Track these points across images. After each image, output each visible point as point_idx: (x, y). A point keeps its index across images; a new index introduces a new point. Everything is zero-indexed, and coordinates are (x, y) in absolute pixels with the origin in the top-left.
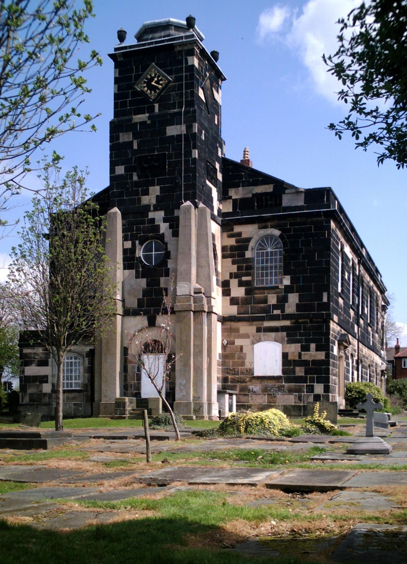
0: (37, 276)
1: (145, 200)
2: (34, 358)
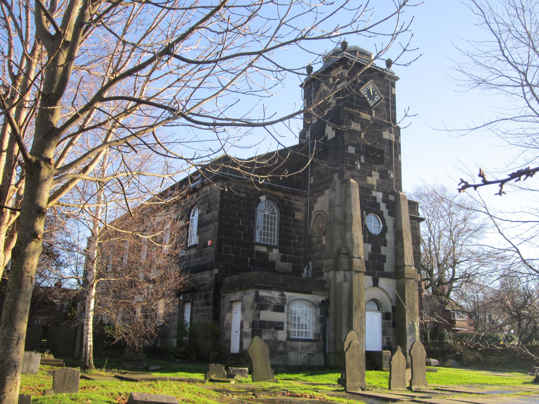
0: (46, 278)
2: (270, 302)
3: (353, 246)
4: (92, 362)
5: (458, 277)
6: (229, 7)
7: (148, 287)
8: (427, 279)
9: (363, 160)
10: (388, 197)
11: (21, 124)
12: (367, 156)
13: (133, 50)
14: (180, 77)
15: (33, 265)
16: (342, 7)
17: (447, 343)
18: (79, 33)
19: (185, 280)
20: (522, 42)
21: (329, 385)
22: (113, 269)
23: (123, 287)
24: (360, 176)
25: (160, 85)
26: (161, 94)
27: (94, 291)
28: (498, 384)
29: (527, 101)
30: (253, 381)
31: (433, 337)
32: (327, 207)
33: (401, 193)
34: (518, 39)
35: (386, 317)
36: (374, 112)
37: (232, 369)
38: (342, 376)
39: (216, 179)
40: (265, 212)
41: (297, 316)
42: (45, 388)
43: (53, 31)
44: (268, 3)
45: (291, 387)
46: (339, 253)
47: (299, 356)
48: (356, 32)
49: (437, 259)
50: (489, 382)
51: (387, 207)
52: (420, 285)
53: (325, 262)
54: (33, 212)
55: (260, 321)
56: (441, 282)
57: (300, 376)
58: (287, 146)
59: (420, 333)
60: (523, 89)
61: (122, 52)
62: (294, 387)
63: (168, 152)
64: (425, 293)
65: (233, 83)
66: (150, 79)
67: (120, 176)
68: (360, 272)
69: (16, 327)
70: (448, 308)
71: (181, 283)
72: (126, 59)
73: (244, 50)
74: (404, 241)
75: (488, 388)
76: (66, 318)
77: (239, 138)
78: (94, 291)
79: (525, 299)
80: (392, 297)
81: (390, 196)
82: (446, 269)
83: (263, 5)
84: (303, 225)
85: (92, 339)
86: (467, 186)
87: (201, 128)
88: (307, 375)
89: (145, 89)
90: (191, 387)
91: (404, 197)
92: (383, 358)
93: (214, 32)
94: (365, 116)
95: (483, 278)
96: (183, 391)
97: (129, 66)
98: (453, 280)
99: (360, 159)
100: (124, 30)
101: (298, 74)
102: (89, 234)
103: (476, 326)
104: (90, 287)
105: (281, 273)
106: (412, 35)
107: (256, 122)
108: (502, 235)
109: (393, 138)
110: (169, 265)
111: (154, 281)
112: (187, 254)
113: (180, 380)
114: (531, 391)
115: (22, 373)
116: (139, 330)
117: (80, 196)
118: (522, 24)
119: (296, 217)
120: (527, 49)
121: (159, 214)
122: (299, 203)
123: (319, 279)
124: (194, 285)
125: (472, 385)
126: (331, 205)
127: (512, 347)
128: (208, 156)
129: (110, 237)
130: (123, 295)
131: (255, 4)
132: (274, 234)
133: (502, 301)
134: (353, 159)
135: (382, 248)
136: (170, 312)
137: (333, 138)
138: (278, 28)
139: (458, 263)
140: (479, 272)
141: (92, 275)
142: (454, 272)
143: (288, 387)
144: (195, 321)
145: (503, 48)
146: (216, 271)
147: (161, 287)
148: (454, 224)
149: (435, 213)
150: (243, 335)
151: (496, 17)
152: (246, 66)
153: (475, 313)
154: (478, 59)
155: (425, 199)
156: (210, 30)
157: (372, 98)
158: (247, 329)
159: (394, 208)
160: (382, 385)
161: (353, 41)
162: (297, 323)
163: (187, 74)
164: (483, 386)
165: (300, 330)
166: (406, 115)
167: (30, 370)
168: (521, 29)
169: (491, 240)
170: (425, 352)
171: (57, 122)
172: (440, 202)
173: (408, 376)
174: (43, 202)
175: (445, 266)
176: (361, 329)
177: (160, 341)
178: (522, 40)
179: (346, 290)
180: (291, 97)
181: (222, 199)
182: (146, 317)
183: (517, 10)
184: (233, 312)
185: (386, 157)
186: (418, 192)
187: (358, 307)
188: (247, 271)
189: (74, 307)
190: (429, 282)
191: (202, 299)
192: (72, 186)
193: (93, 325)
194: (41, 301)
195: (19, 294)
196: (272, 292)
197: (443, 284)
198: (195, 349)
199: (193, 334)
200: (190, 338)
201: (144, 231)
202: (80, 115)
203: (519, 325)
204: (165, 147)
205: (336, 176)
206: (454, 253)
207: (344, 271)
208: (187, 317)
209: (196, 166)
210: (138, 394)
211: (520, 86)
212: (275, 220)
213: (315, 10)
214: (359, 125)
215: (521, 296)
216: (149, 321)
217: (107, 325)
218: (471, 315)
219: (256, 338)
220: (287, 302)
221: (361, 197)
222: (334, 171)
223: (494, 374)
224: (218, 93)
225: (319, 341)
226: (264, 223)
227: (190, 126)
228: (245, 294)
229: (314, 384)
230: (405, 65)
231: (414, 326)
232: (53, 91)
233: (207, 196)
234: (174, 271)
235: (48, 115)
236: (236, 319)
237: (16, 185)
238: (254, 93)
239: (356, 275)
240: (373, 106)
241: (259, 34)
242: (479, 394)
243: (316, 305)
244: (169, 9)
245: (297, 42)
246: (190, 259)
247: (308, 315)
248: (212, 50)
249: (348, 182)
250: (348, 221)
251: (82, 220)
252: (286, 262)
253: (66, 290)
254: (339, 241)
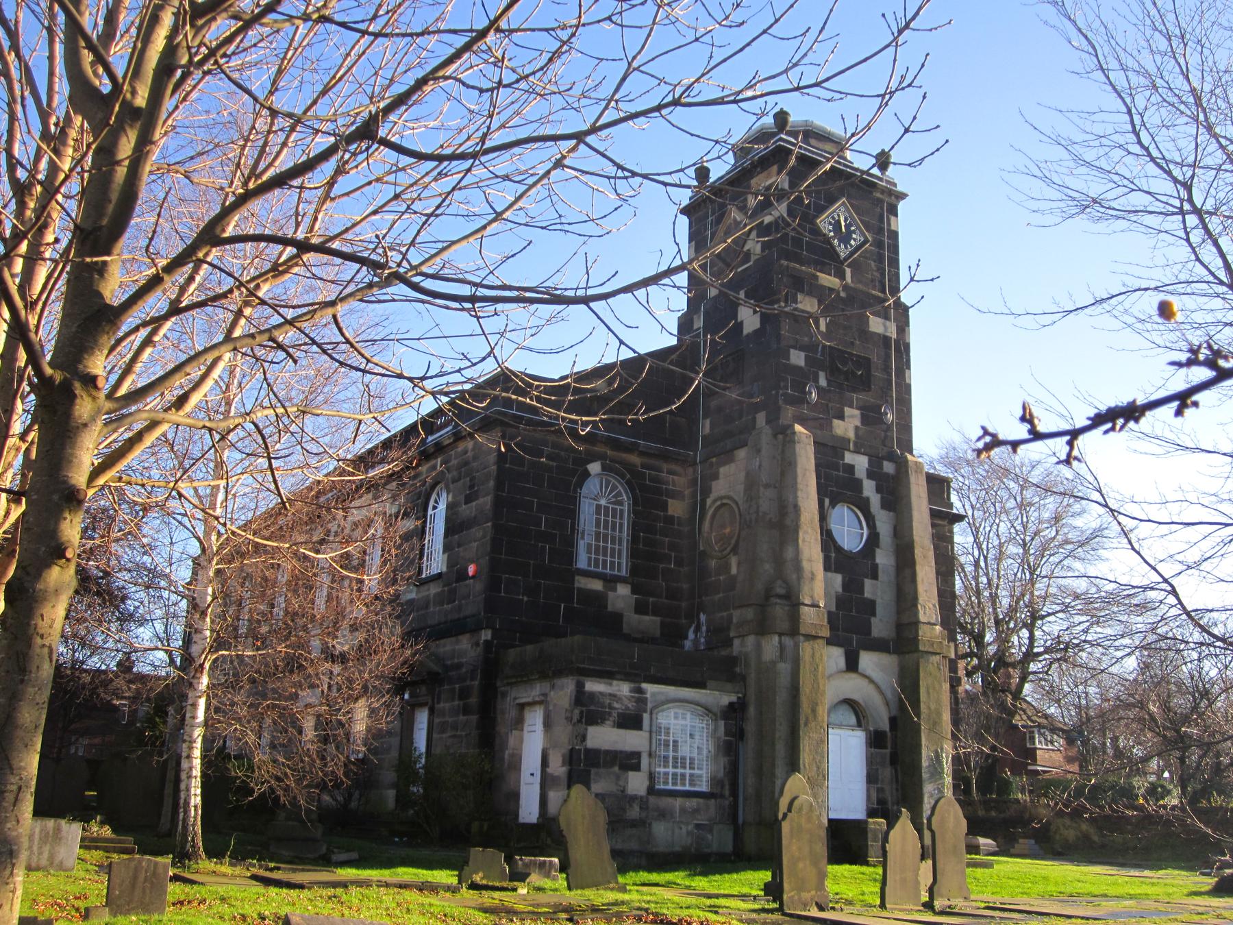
0: (95, 649)
2: (611, 707)
3: (799, 578)
4: (200, 844)
5: (1042, 649)
6: (512, 31)
7: (331, 672)
8: (971, 655)
9: (823, 382)
10: (881, 467)
11: (35, 297)
12: (833, 372)
13: (293, 129)
14: (399, 190)
15: (53, 620)
16: (765, 32)
17: (1017, 801)
18: (165, 89)
19: (414, 655)
20: (1182, 113)
21: (743, 897)
22: (249, 629)
23: (272, 670)
24: (816, 419)
25: (356, 206)
26: (357, 229)
27: (205, 680)
28: (1131, 897)
29: (1193, 249)
30: (570, 888)
31: (984, 788)
32: (741, 488)
33: (909, 457)
34: (1173, 105)
35: (875, 740)
36: (848, 271)
37: (521, 860)
38: (774, 876)
39: (486, 425)
40: (599, 500)
41: (671, 739)
42: (88, 904)
43: (105, 86)
44: (599, 21)
45: (657, 903)
46: (768, 594)
47: (677, 831)
48: (798, 89)
49: (995, 609)
50: (1112, 891)
51: (879, 490)
52: (953, 667)
53: (736, 615)
54: (55, 497)
55: (588, 751)
56: (1002, 660)
57: (678, 877)
58: (642, 352)
59: (954, 779)
60: (1184, 221)
61: (269, 132)
62: (663, 902)
63: (368, 361)
64: (966, 685)
65: (520, 204)
66: (332, 195)
67: (259, 415)
68: (816, 637)
69: (15, 763)
70: (1018, 721)
71: (405, 663)
72: (277, 148)
73: (549, 130)
74: (918, 568)
75: (1108, 906)
76: (141, 742)
77: (533, 331)
78: (205, 680)
79: (1195, 700)
80: (889, 695)
81: (885, 463)
82: (1015, 630)
83: (581, 28)
84: (686, 529)
85: (199, 791)
86: (996, 442)
87: (448, 308)
88: (695, 875)
89: (320, 217)
90: (427, 901)
91: (918, 466)
92: (870, 835)
93: (473, 87)
94: (828, 280)
95: (1098, 651)
96: (408, 910)
97: (285, 162)
98: (1030, 656)
99: (816, 380)
100: (274, 82)
101: (665, 184)
102: (194, 548)
103: (1083, 760)
104: (196, 671)
105: (636, 640)
106: (924, 97)
107: (570, 293)
108: (1138, 553)
109: (892, 332)
110: (378, 621)
111: (343, 658)
112: (420, 595)
113: (401, 886)
114: (1207, 913)
115: (29, 868)
116: (307, 769)
117: (176, 462)
118: (1182, 72)
119: (670, 512)
120: (1192, 129)
121: (356, 503)
122: (678, 479)
123: (724, 653)
124: (435, 667)
125: (1072, 897)
126: (751, 484)
127: (1162, 811)
128: (459, 371)
129: (243, 556)
130: (273, 689)
131: (564, 28)
132: (620, 551)
133: (1142, 705)
134: (801, 378)
135: (868, 583)
136: (380, 730)
137: (756, 332)
138: (624, 79)
139: (1043, 617)
140: (1089, 638)
141: (200, 642)
142: (1032, 638)
143: (649, 902)
144: (437, 750)
145: (1138, 128)
146: (486, 635)
147: (360, 672)
148: (1032, 528)
149: (989, 503)
150: (546, 781)
151: (1122, 55)
152: (549, 165)
153: (1081, 733)
154: (1081, 151)
155: (966, 470)
156: (464, 84)
157: (845, 239)
158: (557, 767)
159: (894, 492)
160: (866, 897)
161: (801, 111)
162: (671, 754)
163: (415, 183)
164: (1097, 901)
165: (679, 771)
166: (912, 280)
167: (57, 862)
168: (1179, 82)
169: (1116, 566)
170: (964, 822)
171: (113, 291)
172: (1000, 479)
173: (925, 878)
174: (79, 477)
175: (1012, 625)
176: (818, 768)
177: (356, 794)
178: (1182, 107)
179: (784, 680)
180: (656, 234)
181: (500, 470)
182: (325, 740)
183: (1169, 40)
184: (526, 728)
185: (877, 374)
186: (951, 455)
187: (810, 718)
188: (560, 634)
189: (160, 717)
190: (975, 661)
191: (453, 700)
192: (149, 440)
193: (203, 757)
194: (80, 703)
195: (20, 687)
196: (615, 682)
197: (1007, 665)
198: (435, 811)
199: (432, 778)
200: (425, 789)
201: (322, 542)
202: (166, 278)
203: (1182, 760)
204: (363, 351)
205: (761, 418)
206: (1032, 594)
207: (780, 635)
208: (420, 740)
209: (433, 394)
210: (302, 917)
211: (1176, 214)
212: (621, 517)
213: (707, 39)
214: (816, 302)
215: (1185, 694)
216: (332, 748)
217: (236, 757)
218: (1071, 736)
219: (578, 789)
220: (649, 705)
221: (818, 466)
222: (756, 408)
223: (1124, 872)
224: (484, 227)
225: (722, 796)
226: (598, 525)
227: (423, 302)
228: (553, 687)
229: (709, 896)
230: (909, 165)
231: (939, 762)
232: (105, 222)
233: (466, 463)
234: (390, 636)
235: (92, 277)
236: (533, 744)
237: (23, 437)
238: (567, 227)
239: (806, 644)
240: (846, 259)
241: (576, 91)
242: (1087, 919)
243: (715, 714)
244: (376, 35)
245: (664, 112)
246: (427, 607)
247: (697, 737)
248: (473, 128)
249: (789, 432)
250: (788, 522)
251: (179, 517)
252: (646, 614)
253: (142, 678)
254: (768, 567)
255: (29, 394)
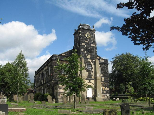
1: (88, 57)
255: (150, 99)
